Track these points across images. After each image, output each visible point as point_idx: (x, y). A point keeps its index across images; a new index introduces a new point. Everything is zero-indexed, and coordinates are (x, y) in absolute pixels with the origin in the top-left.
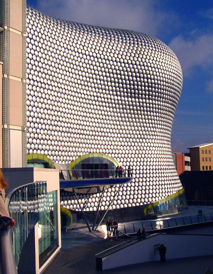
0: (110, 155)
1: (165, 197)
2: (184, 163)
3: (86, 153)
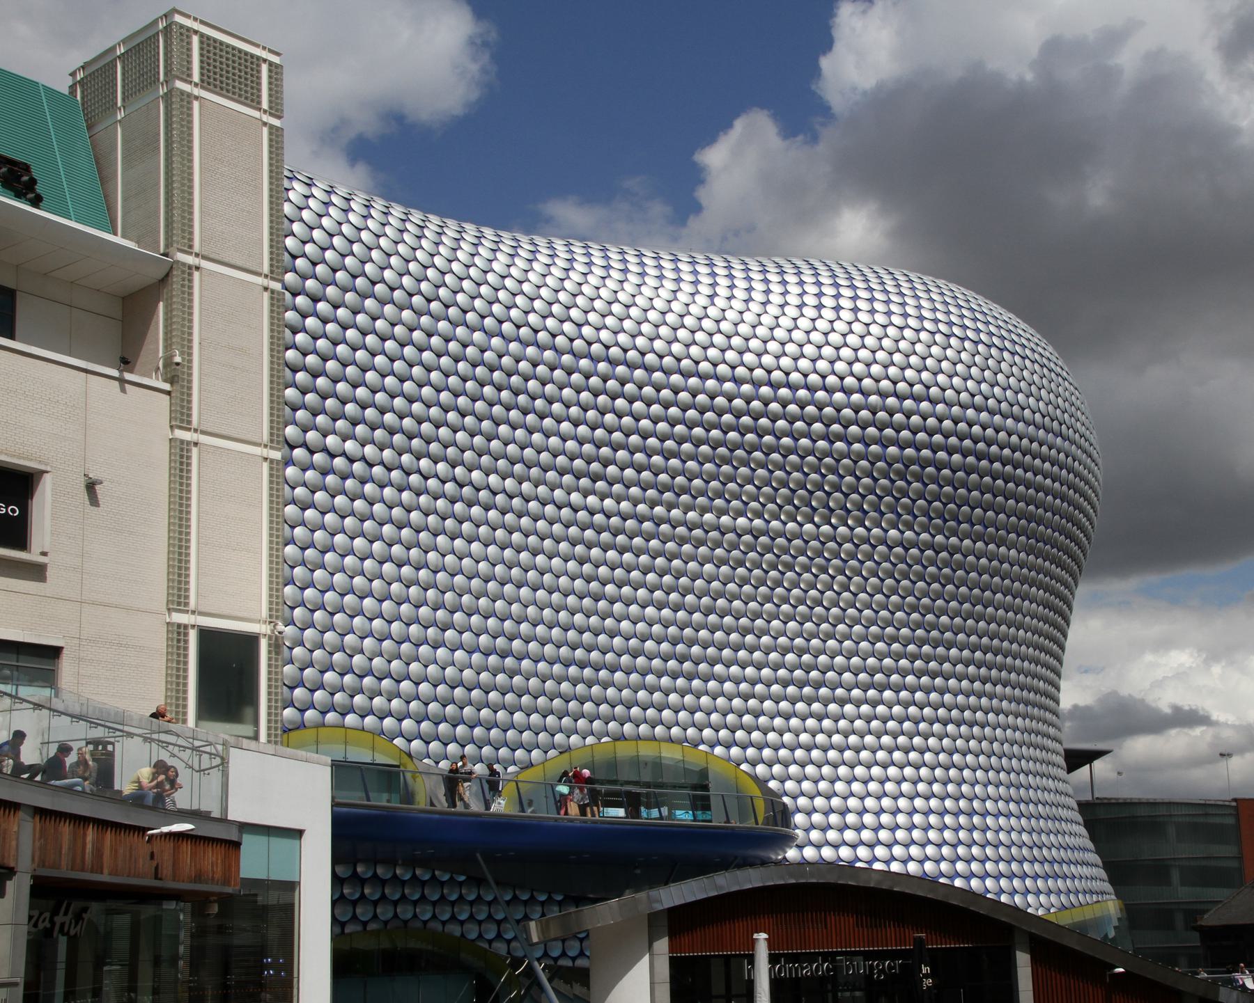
0: (719, 750)
3: (599, 739)
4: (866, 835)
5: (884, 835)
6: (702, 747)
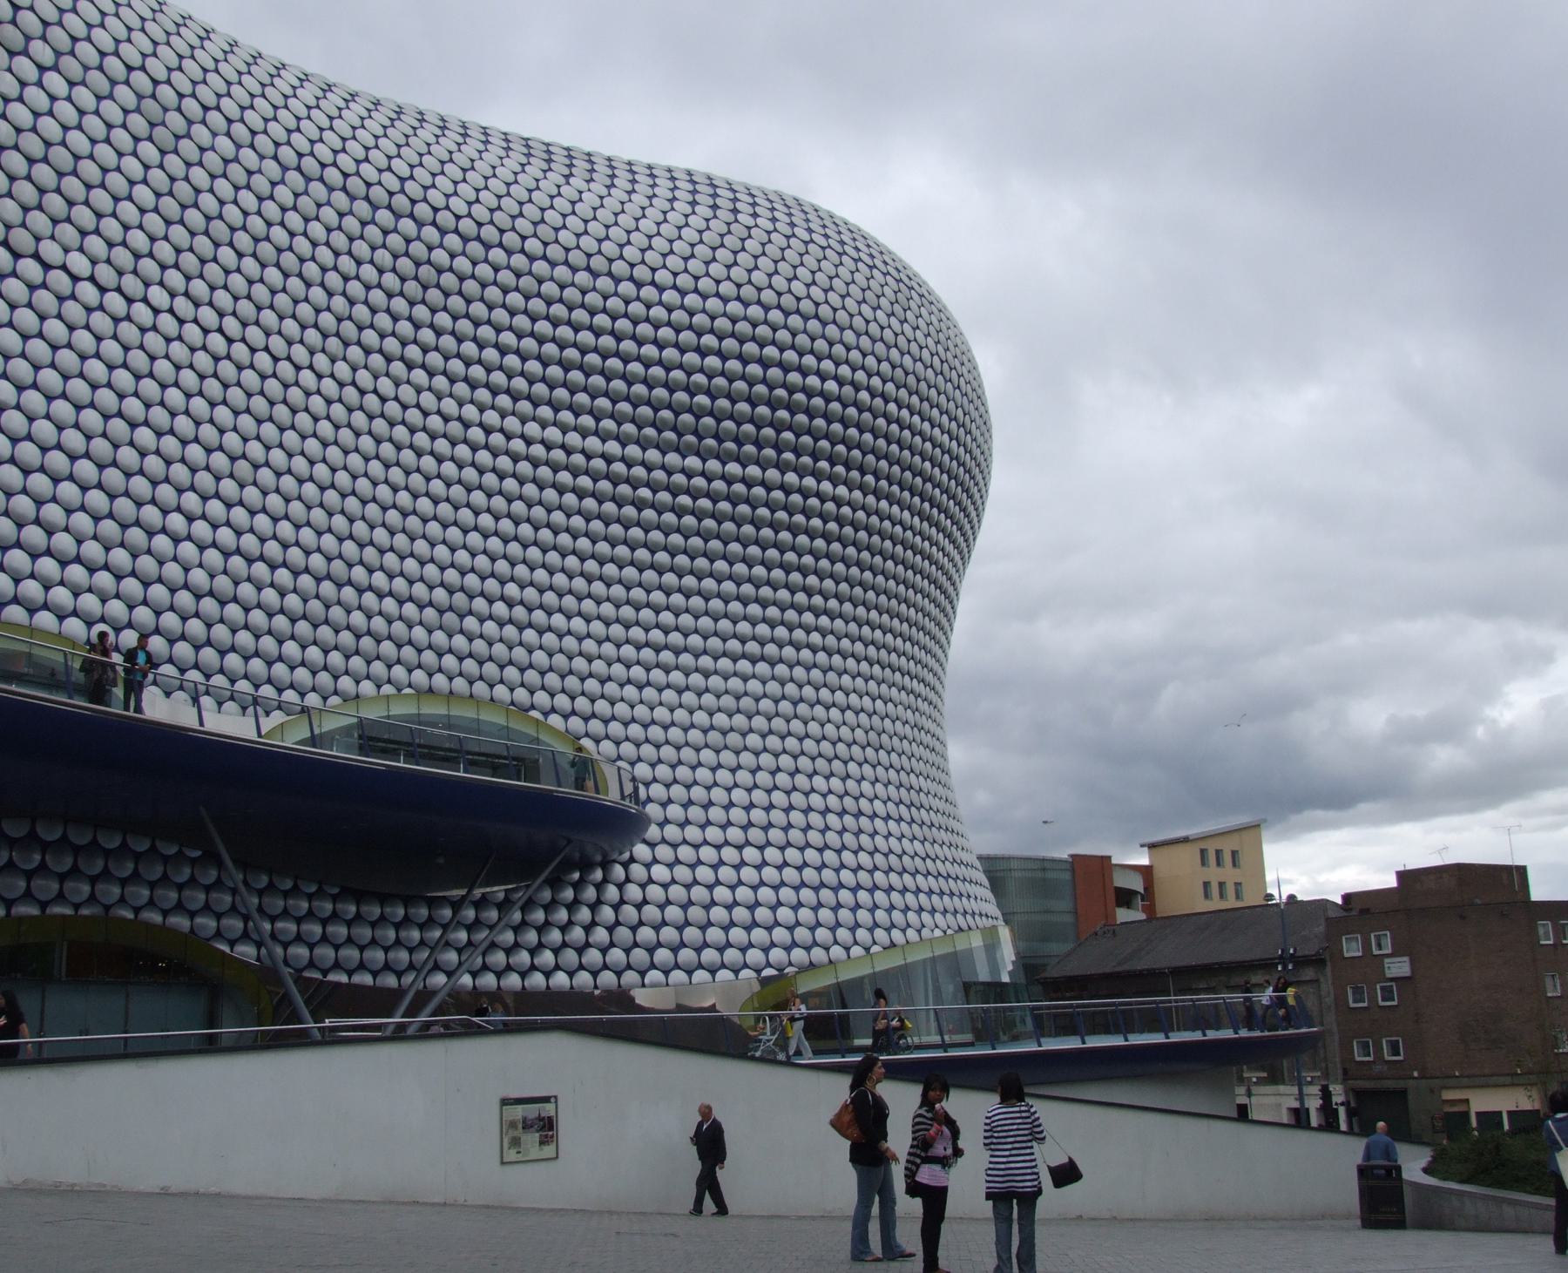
0: (555, 720)
1: (867, 950)
2: (1111, 896)
4: (734, 834)
5: (755, 835)
6: (534, 714)
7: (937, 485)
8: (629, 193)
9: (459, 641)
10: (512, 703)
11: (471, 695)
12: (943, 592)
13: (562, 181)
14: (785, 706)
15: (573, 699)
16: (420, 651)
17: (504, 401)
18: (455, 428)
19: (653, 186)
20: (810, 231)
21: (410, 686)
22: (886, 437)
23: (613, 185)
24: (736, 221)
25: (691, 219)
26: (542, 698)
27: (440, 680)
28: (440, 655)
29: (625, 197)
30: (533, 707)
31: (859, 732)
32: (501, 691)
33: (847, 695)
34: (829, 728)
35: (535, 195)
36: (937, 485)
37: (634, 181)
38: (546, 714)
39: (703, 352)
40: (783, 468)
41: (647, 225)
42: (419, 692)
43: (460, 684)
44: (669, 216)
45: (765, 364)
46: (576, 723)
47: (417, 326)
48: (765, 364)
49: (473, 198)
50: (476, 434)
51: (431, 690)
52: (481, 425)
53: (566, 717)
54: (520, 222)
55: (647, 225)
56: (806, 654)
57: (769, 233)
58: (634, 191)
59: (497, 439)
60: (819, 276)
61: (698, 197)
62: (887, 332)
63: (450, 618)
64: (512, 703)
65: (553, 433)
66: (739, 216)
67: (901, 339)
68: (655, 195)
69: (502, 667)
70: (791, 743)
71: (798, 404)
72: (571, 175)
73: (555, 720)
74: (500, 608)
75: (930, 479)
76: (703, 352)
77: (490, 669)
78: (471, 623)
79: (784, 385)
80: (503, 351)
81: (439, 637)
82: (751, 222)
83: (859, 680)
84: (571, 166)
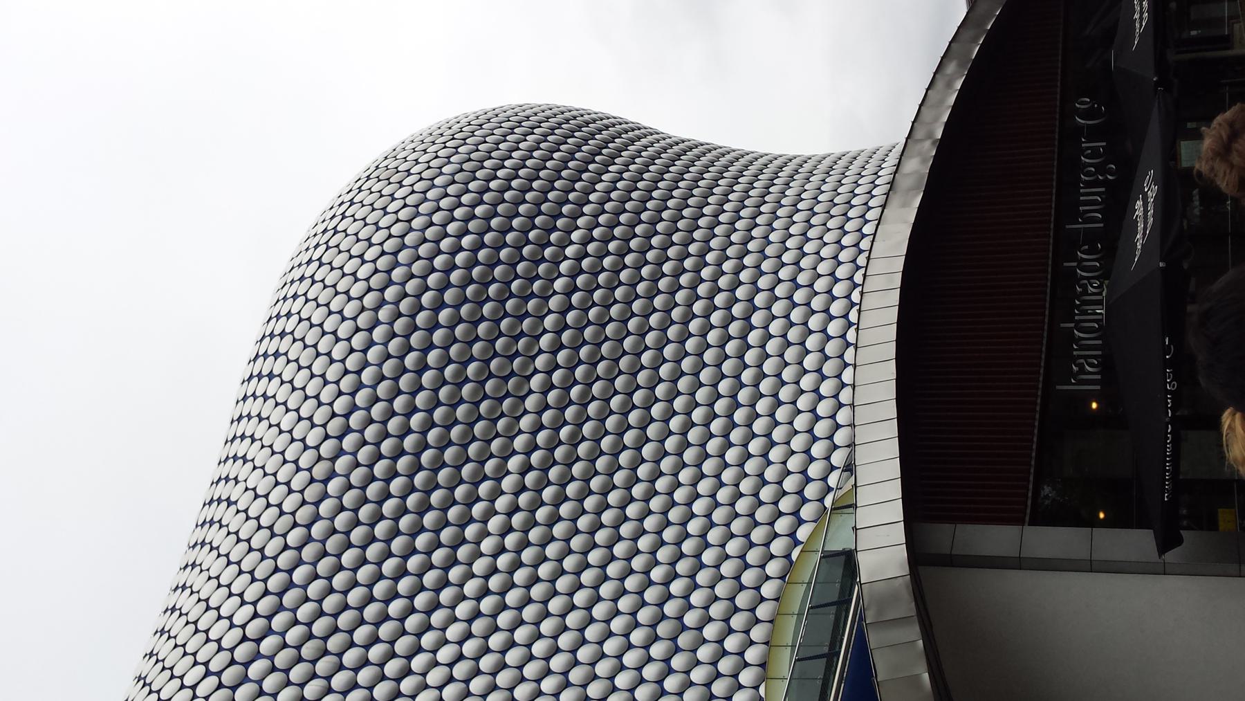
0: (803, 533)
6: (794, 556)
7: (579, 147)
8: (261, 419)
9: (710, 631)
10: (782, 578)
11: (777, 600)
12: (682, 157)
13: (233, 508)
14: (799, 296)
15: (776, 535)
16: (719, 675)
17: (455, 574)
18: (478, 626)
19: (249, 417)
20: (309, 262)
21: (756, 688)
22: (524, 191)
23: (244, 457)
24: (286, 354)
25: (292, 356)
26: (777, 547)
27: (752, 655)
28: (725, 653)
29: (257, 444)
30: (788, 556)
31: (830, 224)
32: (768, 590)
33: (787, 249)
34: (825, 252)
35: (303, 363)
36: (579, 147)
37: (243, 437)
38: (797, 543)
39: (422, 368)
40: (502, 472)
41: (287, 421)
42: (763, 678)
43: (757, 633)
44: (280, 400)
45: (439, 305)
46: (807, 512)
47: (366, 662)
48: (439, 305)
49: (338, 317)
50: (487, 604)
51: (763, 665)
52: (478, 600)
53: (801, 522)
54: (325, 398)
55: (287, 421)
56: (699, 507)
57: (307, 301)
58: (252, 436)
59: (494, 583)
60: (347, 270)
61: (265, 372)
62: (417, 187)
63: (683, 640)
64: (782, 578)
65: (494, 524)
66: (282, 351)
67: (425, 175)
68: (259, 415)
69: (742, 588)
70: (823, 408)
71: (461, 353)
72: (228, 499)
73: (803, 533)
74: (676, 587)
75: (572, 153)
76: (422, 368)
77: (742, 600)
78: (690, 619)
79: (463, 287)
80: (402, 572)
81: (704, 653)
82: (295, 318)
83: (772, 237)
84: (219, 501)
